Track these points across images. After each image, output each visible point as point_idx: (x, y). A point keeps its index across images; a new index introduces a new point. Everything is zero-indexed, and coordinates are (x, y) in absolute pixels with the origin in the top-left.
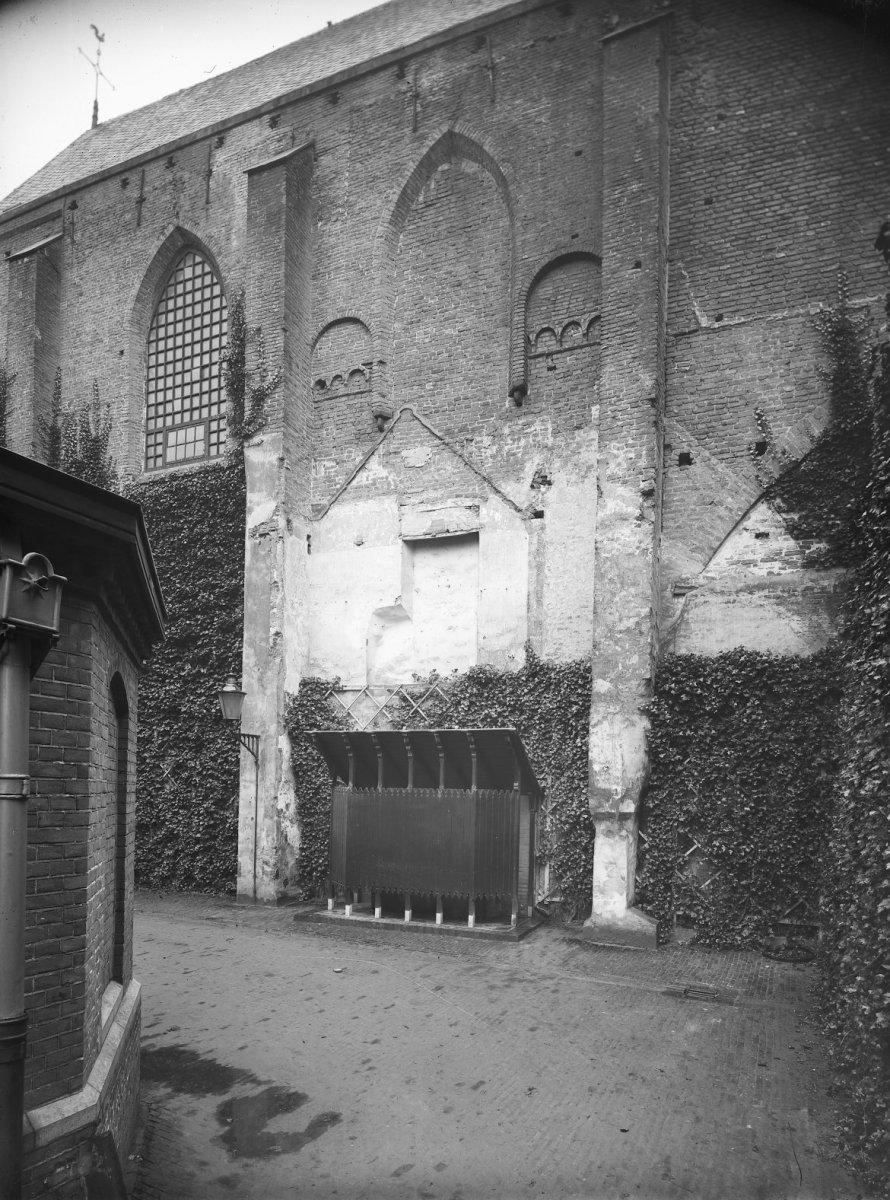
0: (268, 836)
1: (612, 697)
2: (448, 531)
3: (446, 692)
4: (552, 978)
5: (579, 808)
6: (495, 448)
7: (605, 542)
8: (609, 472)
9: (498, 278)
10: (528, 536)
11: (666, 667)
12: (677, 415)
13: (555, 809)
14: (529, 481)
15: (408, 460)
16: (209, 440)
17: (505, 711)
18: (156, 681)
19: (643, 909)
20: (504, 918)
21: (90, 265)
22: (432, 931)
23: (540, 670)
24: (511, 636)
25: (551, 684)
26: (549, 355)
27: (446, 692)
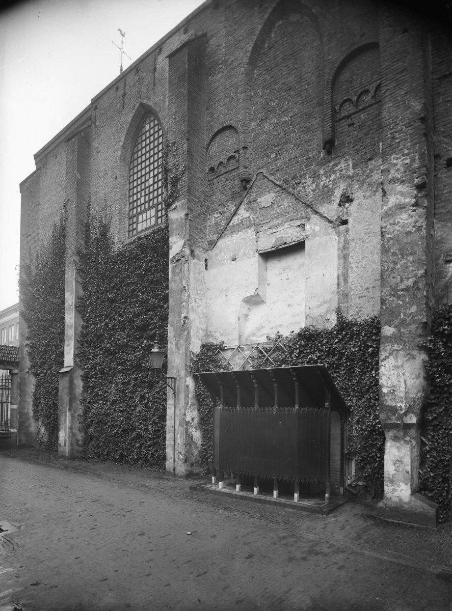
0: (181, 437)
1: (395, 339)
2: (286, 243)
3: (285, 345)
4: (343, 552)
5: (374, 420)
6: (314, 185)
7: (388, 227)
8: (390, 177)
9: (314, 78)
10: (337, 238)
11: (441, 314)
12: (443, 132)
13: (358, 421)
14: (338, 201)
15: (261, 204)
16: (157, 215)
17: (322, 355)
18: (131, 351)
19: (425, 495)
20: (320, 495)
21: (103, 136)
22: (270, 502)
23: (346, 326)
24: (327, 306)
25: (354, 335)
26: (349, 117)
27: (285, 345)
